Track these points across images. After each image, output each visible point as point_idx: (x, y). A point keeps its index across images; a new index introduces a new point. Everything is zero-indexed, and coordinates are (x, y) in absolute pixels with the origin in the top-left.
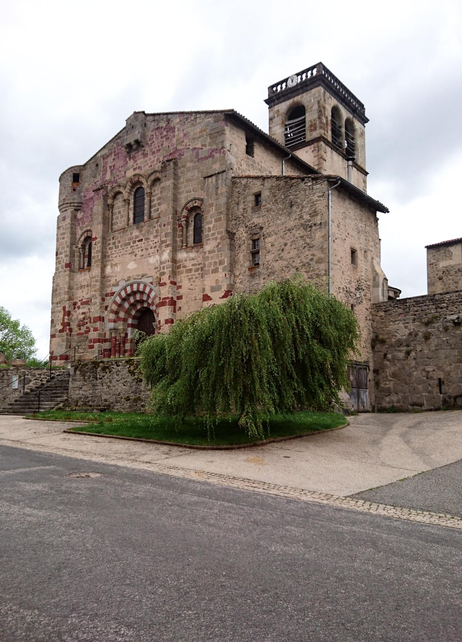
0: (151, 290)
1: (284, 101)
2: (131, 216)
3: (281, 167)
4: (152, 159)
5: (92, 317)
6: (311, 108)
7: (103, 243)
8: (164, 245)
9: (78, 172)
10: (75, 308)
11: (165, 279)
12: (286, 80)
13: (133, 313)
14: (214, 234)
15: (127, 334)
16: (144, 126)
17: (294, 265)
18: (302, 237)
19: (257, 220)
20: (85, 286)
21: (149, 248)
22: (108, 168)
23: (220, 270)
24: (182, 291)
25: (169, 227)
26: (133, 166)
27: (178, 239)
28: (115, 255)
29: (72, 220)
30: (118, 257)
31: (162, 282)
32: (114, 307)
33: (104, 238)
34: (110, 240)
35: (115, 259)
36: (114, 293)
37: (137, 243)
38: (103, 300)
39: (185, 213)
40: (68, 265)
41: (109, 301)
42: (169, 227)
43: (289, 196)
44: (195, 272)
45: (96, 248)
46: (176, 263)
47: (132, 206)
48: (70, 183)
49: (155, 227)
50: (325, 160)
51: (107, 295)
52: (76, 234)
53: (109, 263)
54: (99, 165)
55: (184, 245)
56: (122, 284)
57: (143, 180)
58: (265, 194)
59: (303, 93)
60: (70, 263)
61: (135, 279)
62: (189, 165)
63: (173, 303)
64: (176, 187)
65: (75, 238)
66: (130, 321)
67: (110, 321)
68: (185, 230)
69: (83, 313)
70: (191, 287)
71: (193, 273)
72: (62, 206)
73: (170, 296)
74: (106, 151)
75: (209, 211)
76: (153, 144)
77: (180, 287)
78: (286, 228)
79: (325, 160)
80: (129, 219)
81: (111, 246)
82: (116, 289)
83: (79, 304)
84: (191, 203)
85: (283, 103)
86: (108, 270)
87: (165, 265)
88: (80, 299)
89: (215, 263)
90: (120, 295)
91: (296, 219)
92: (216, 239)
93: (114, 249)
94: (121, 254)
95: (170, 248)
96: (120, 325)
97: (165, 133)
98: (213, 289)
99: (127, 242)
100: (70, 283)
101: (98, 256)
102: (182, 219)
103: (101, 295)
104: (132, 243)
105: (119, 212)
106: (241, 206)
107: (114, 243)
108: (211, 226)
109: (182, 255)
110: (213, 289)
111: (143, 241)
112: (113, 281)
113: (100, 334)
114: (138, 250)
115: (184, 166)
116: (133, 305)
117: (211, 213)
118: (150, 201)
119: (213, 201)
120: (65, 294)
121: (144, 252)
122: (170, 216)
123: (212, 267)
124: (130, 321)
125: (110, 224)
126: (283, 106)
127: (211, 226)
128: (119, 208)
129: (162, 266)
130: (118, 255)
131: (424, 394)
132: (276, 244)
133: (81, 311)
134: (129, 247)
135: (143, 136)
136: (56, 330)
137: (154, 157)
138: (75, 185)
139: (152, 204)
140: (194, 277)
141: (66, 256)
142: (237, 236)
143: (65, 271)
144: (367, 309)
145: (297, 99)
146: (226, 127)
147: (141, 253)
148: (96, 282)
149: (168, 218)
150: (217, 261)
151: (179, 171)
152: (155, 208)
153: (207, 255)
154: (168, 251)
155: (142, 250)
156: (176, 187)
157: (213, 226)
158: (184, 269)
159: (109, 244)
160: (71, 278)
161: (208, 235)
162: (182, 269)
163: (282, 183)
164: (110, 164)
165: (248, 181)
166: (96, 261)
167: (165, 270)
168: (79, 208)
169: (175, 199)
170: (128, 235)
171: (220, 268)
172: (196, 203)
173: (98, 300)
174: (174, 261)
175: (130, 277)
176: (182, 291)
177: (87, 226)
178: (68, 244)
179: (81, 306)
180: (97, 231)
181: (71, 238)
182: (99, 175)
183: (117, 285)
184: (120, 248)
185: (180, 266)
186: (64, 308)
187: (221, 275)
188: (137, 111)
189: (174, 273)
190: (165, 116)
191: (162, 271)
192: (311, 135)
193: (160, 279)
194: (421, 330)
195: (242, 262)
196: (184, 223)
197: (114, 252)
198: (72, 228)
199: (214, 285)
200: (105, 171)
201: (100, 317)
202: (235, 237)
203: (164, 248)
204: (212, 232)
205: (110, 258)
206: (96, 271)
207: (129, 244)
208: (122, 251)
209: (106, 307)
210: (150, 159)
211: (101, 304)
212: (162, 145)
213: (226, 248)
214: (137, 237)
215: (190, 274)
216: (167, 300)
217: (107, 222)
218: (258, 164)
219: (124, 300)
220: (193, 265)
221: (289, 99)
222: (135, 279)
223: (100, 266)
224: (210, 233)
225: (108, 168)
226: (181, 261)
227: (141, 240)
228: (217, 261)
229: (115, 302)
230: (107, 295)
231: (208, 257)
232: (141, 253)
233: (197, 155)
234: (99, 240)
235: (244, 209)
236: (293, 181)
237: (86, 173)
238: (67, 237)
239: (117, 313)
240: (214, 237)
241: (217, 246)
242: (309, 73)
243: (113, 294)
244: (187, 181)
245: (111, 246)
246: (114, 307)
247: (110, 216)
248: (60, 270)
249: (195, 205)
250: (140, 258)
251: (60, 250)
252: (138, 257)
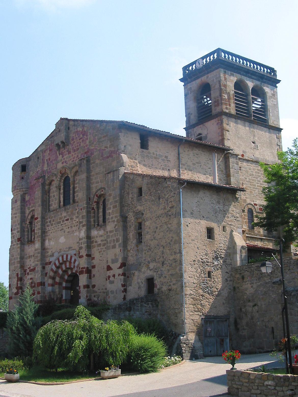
0: (75, 260)
1: (195, 80)
2: (62, 199)
3: (177, 151)
5: (36, 282)
6: (214, 87)
7: (42, 221)
8: (81, 224)
9: (25, 163)
10: (25, 274)
11: (84, 252)
12: (194, 63)
13: (66, 277)
14: (112, 218)
15: (62, 295)
16: (67, 129)
17: (162, 244)
18: (166, 223)
19: (139, 208)
20: (31, 256)
21: (73, 226)
22: (45, 161)
23: (117, 246)
24: (95, 262)
25: (84, 211)
26: (61, 160)
27: (92, 220)
28: (51, 230)
29: (21, 202)
30: (53, 233)
31: (81, 254)
32: (52, 274)
33: (43, 218)
34: (47, 219)
35: (51, 235)
36: (51, 262)
37: (65, 222)
38: (44, 268)
39: (96, 199)
40: (19, 240)
41: (48, 268)
42: (84, 211)
43: (158, 191)
44: (103, 246)
45: (37, 226)
46: (91, 239)
47: (62, 191)
48: (20, 172)
49: (77, 210)
50: (228, 131)
51: (46, 264)
52: (25, 213)
53: (47, 238)
54: (40, 158)
55: (96, 224)
56: (56, 255)
57: (68, 171)
58: (144, 189)
59: (208, 73)
60: (21, 238)
61: (64, 251)
62: (98, 161)
63: (89, 271)
64: (88, 179)
65: (25, 217)
66: (64, 284)
67: (49, 285)
68: (96, 212)
69: (31, 279)
70: (101, 258)
71: (102, 247)
72: (14, 189)
73: (86, 266)
74: (44, 147)
75: (109, 200)
76: (74, 144)
77: (93, 258)
78: (156, 215)
79: (228, 131)
80: (60, 202)
81: (48, 224)
82: (52, 259)
83: (28, 271)
84: (99, 191)
85: (194, 82)
86: (47, 243)
88: (29, 267)
89: (114, 240)
90: (55, 264)
91: (162, 209)
92: (114, 221)
93: (50, 227)
94: (54, 230)
95: (85, 228)
96: (57, 288)
97: (81, 136)
98: (114, 261)
99: (58, 221)
100: (21, 254)
101: (39, 232)
102: (94, 204)
103: (41, 264)
104: (62, 222)
105: (54, 196)
106: (131, 196)
107: (50, 222)
108: (110, 211)
109: (94, 233)
110: (114, 261)
111: (69, 220)
112: (50, 253)
113: (41, 296)
115: (94, 163)
116: (65, 272)
117: (110, 201)
118: (74, 188)
120: (18, 264)
121: (70, 230)
122: (85, 202)
123: (112, 244)
124: (64, 284)
125: (48, 205)
126: (195, 84)
127: (110, 211)
128: (53, 193)
129: (80, 242)
130: (53, 231)
131: (264, 340)
132: (151, 227)
133: (29, 277)
134: (60, 225)
135: (67, 137)
136: (13, 293)
137: (75, 154)
138: (23, 174)
139: (75, 190)
140: (102, 250)
141: (18, 232)
142: (128, 219)
143: (17, 244)
144: (227, 272)
145: (204, 79)
146: (120, 134)
147: (67, 230)
148: (38, 254)
149: (83, 204)
150: (115, 239)
151: (91, 166)
153: (109, 234)
154: (84, 230)
155: (69, 228)
156: (88, 179)
157: (113, 212)
158: (96, 244)
159: (47, 222)
160: (22, 250)
161: (109, 218)
162: (94, 244)
163: (153, 180)
164: (47, 158)
165: (134, 177)
166: (37, 237)
167: (82, 246)
168: (27, 192)
169: (89, 188)
170: (59, 215)
171: (117, 244)
172: (102, 191)
173: (39, 268)
174: (89, 237)
175: (61, 250)
176: (95, 262)
177: (32, 207)
178: (19, 222)
179: (30, 273)
180: (38, 213)
181: (21, 216)
182: (40, 165)
183: (52, 255)
184: (54, 226)
185: (93, 241)
186: (17, 274)
187: (117, 250)
188: (62, 118)
189: (89, 247)
190: (81, 123)
191: (80, 246)
192: (215, 110)
193: (79, 252)
194: (260, 290)
195: (132, 240)
196: (95, 207)
197: (50, 229)
198: (21, 209)
199: (114, 258)
200: (44, 163)
201: (41, 282)
202: (128, 220)
203: (81, 228)
204: (111, 216)
205: (48, 234)
206: (37, 245)
207: (60, 222)
208: (55, 228)
209: (46, 274)
210: (72, 155)
211: (42, 272)
212: (80, 145)
213: (121, 229)
214: (65, 217)
215: (99, 248)
216: (84, 270)
217: (46, 205)
218: (153, 154)
219: (58, 268)
221: (198, 78)
222: (64, 251)
223: (40, 240)
224: (110, 217)
225: (45, 161)
226: (94, 237)
227: (67, 220)
228: (115, 239)
229: (52, 270)
230: (46, 264)
231: (109, 235)
232: (67, 230)
233: (102, 156)
234: (39, 219)
235: (132, 198)
236: (160, 180)
237: (31, 163)
238: (19, 215)
239: (54, 278)
240: (113, 220)
241: (115, 227)
242: (208, 58)
243: (50, 263)
244: (97, 174)
245: (48, 224)
246: (52, 274)
247: (48, 199)
248: (14, 243)
249: (102, 193)
250: (67, 234)
251: (14, 227)
252: (66, 233)
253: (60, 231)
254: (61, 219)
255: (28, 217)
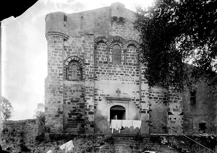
4: (130, 33)
37: (119, 75)
71: (158, 99)
87: (145, 92)
105: (101, 53)
114: (120, 79)
119: (88, 74)
134: (113, 76)
152: (129, 60)
158: (153, 97)
191: (142, 95)
207: (113, 74)
214: (119, 72)
220: (158, 96)
253: (113, 80)
254: (113, 71)
255: (68, 60)
